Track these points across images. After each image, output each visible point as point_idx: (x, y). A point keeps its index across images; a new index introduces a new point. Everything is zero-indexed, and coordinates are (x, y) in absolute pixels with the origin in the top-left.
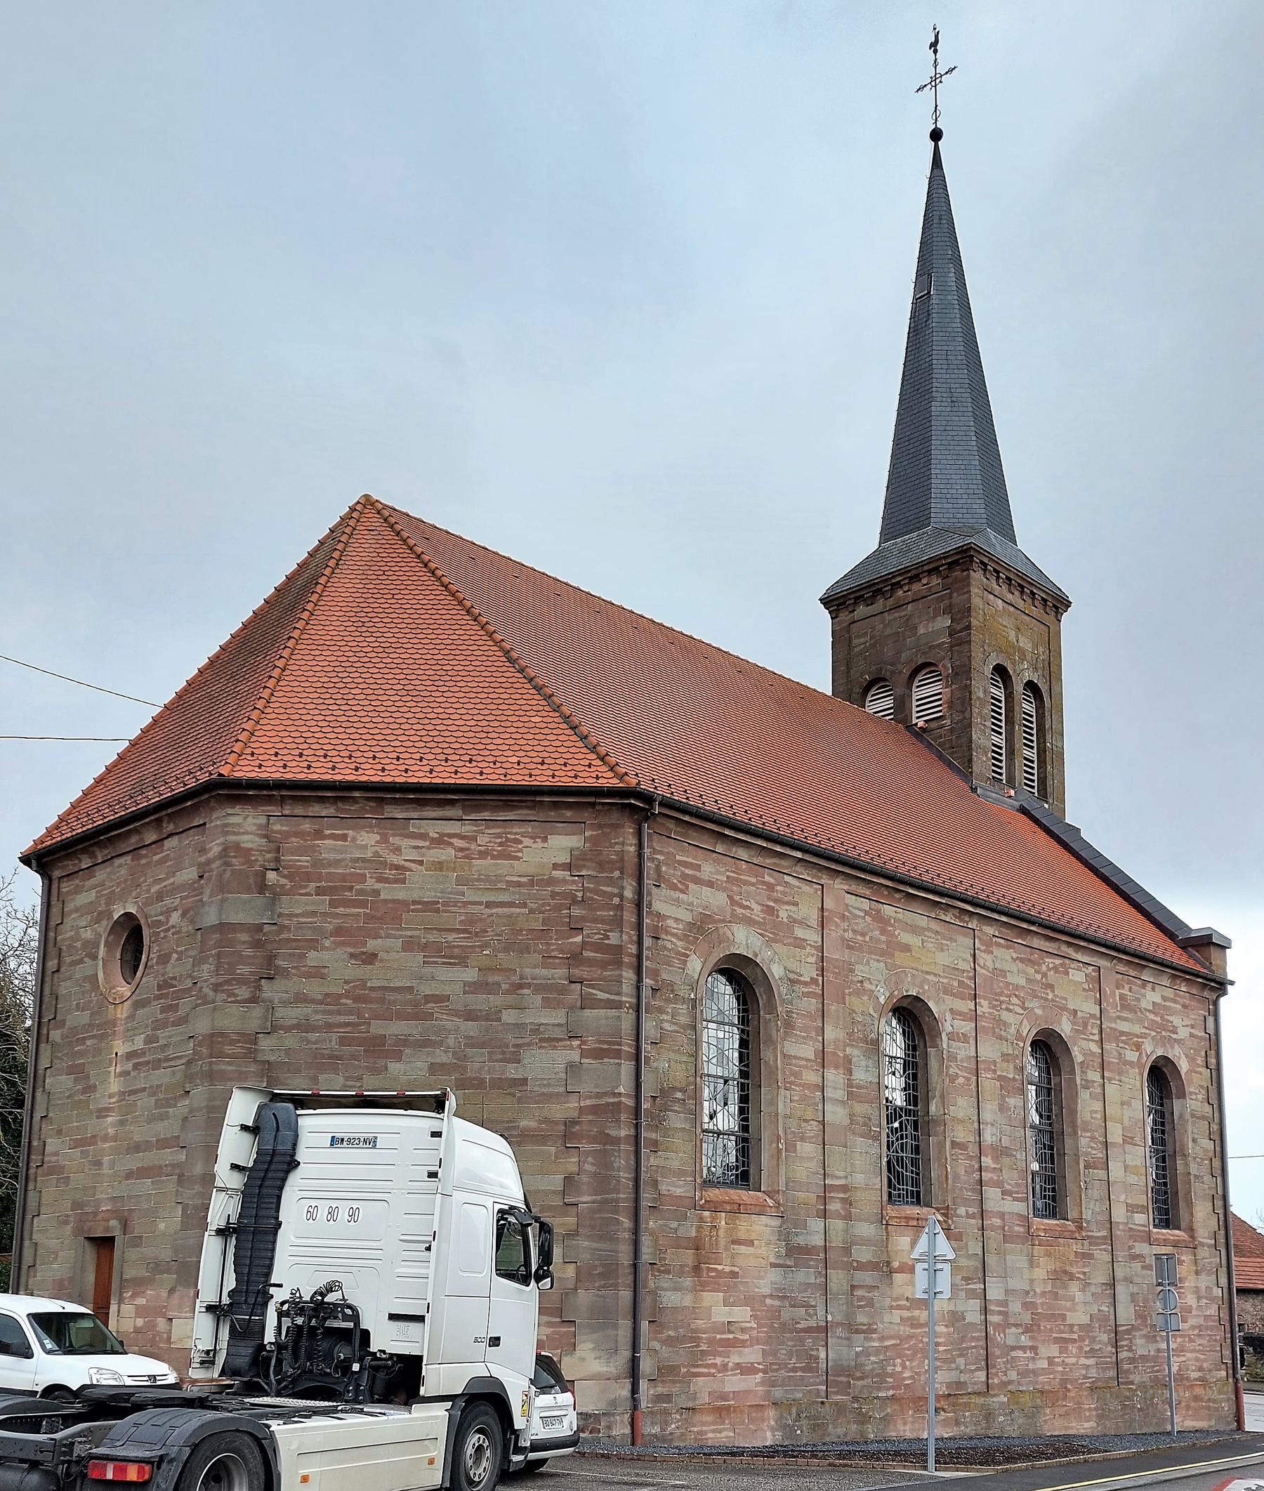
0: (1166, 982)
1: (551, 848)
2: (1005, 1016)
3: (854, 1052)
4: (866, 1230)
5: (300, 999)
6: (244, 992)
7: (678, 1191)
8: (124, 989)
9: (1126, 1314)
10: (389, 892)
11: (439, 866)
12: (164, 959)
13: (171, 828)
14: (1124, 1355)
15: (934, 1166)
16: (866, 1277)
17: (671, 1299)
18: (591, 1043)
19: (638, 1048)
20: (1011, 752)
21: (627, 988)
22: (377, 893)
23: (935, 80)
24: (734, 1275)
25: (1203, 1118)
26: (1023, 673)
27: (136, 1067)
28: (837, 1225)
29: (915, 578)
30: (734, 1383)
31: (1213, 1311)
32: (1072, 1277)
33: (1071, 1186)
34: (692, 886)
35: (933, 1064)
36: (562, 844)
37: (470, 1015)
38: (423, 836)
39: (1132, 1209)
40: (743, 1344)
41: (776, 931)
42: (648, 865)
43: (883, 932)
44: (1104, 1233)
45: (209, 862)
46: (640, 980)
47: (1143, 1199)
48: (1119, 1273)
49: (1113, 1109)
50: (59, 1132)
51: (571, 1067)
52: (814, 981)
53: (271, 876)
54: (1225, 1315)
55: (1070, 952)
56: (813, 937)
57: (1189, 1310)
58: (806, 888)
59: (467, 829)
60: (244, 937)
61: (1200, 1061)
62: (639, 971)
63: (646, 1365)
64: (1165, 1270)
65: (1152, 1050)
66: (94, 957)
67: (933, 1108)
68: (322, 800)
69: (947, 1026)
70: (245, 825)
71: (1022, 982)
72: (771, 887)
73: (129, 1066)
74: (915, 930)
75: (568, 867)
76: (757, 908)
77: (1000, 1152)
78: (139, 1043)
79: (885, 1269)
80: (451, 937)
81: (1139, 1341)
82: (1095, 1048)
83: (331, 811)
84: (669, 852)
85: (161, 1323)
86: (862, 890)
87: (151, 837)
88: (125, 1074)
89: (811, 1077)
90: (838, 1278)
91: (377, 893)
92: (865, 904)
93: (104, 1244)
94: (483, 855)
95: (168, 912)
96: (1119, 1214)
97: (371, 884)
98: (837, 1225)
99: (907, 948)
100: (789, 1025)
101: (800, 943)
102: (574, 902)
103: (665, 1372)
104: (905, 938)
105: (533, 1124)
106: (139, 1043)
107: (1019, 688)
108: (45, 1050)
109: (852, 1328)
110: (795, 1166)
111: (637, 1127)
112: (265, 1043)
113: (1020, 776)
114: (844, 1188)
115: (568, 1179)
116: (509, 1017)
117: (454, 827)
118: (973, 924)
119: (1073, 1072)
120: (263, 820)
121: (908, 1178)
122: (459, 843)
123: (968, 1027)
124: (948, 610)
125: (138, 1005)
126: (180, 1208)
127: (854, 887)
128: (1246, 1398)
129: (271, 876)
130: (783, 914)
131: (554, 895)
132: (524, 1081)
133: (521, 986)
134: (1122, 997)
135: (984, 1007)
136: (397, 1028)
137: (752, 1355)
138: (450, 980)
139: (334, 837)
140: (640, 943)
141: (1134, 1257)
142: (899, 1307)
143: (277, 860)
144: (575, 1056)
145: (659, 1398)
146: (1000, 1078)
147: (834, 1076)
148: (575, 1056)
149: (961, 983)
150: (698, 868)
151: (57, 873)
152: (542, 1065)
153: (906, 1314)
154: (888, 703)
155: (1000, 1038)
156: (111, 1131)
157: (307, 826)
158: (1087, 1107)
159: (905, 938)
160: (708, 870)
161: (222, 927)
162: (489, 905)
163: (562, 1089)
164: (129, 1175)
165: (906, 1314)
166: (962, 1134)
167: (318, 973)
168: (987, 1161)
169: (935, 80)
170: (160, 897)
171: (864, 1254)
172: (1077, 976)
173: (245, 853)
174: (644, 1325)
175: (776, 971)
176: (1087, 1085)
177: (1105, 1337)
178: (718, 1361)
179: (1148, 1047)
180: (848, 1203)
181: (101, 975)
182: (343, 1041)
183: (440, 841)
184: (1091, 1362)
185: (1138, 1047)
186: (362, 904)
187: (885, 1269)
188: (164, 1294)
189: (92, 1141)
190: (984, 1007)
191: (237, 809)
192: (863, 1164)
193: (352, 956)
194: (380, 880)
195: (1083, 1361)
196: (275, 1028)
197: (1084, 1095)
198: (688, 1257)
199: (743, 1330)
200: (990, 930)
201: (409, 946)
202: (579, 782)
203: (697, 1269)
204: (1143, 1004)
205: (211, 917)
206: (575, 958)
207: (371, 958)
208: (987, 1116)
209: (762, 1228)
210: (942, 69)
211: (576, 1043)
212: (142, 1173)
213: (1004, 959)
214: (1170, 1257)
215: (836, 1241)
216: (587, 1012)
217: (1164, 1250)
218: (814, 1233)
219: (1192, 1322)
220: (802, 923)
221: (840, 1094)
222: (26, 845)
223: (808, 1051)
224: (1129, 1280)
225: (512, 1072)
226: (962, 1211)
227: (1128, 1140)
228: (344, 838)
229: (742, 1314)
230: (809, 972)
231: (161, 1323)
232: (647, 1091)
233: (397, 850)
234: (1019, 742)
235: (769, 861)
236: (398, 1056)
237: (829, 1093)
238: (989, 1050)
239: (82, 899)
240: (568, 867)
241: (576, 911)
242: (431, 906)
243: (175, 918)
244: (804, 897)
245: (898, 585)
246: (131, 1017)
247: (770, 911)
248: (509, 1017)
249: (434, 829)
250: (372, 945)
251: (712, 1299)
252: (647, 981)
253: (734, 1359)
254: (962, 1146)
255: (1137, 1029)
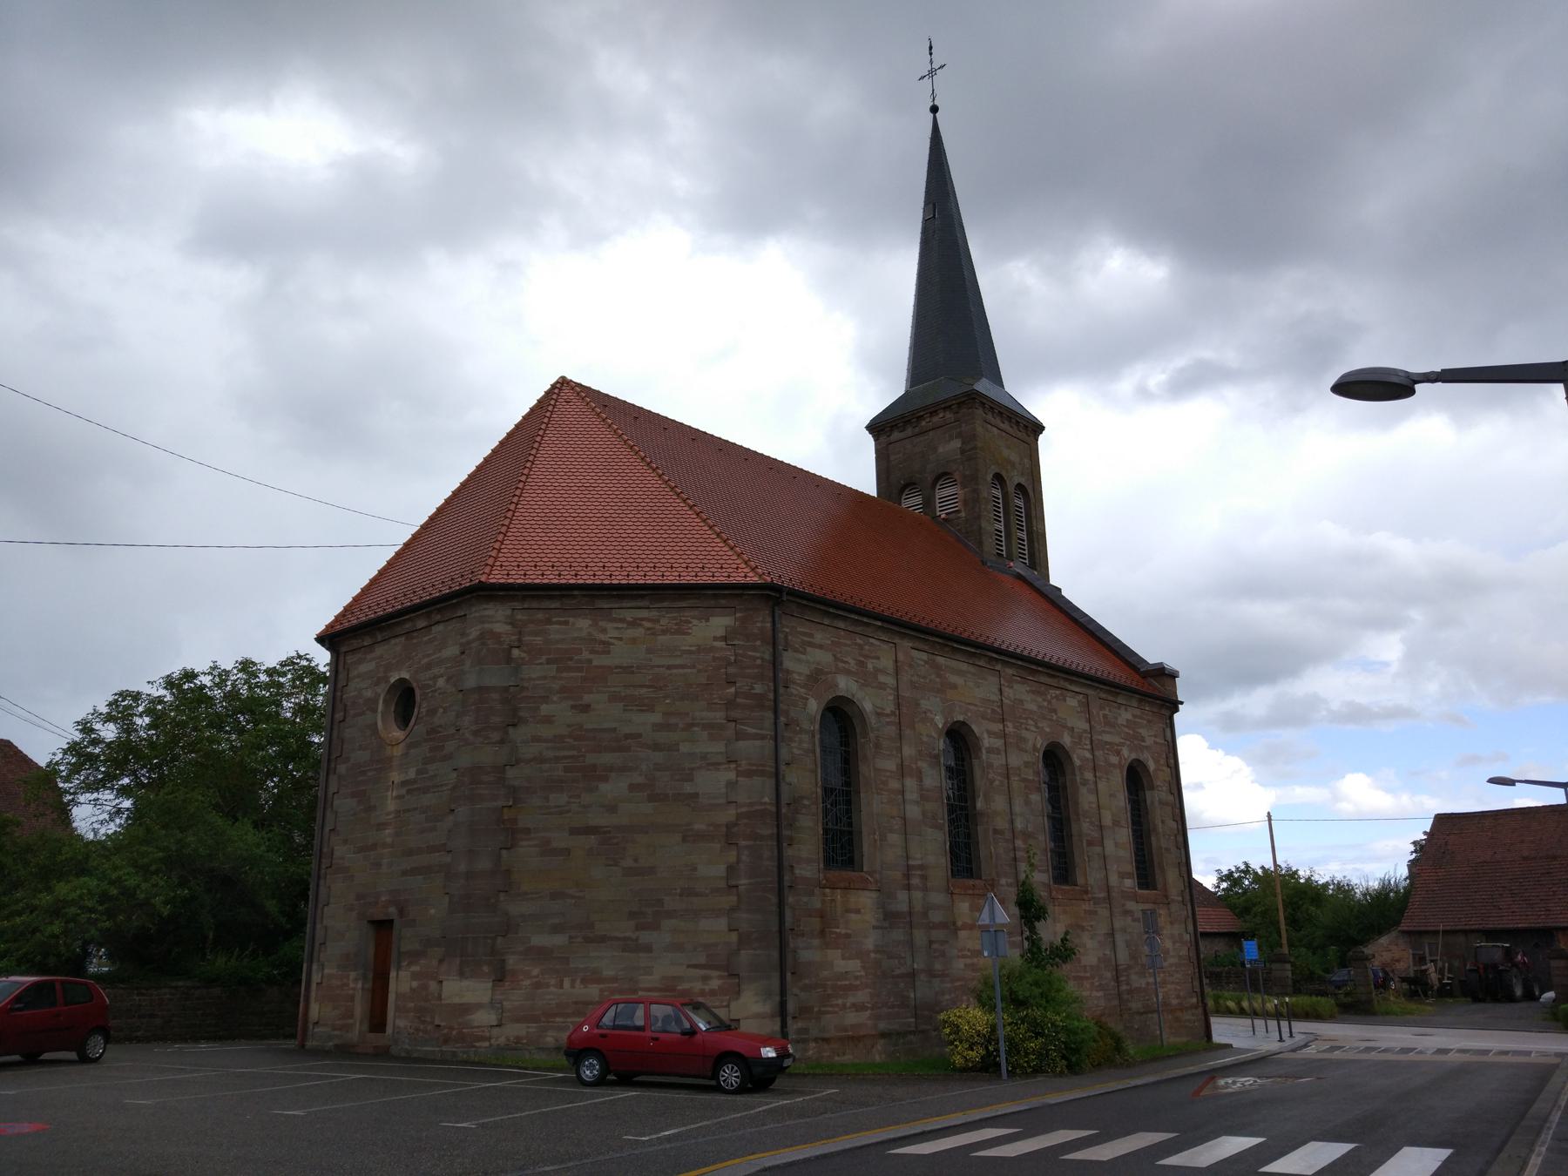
0: (1135, 704)
1: (714, 627)
2: (1025, 734)
3: (923, 765)
4: (938, 898)
5: (536, 739)
6: (496, 736)
7: (808, 874)
8: (398, 734)
9: (1123, 956)
10: (599, 661)
11: (634, 641)
12: (432, 712)
13: (438, 617)
14: (1124, 987)
15: (982, 847)
16: (938, 934)
17: (806, 955)
18: (744, 765)
19: (777, 768)
20: (1008, 535)
21: (769, 723)
22: (590, 661)
23: (932, 73)
24: (848, 936)
25: (1167, 804)
26: (1014, 478)
27: (408, 792)
28: (917, 895)
29: (932, 414)
30: (851, 1018)
31: (1184, 952)
32: (1083, 929)
33: (1077, 860)
34: (809, 649)
35: (978, 773)
36: (720, 623)
37: (656, 747)
38: (622, 620)
39: (1122, 875)
40: (856, 988)
41: (867, 679)
42: (781, 636)
43: (938, 676)
44: (1102, 895)
45: (469, 643)
46: (776, 718)
47: (1130, 867)
48: (1117, 925)
49: (1102, 799)
50: (345, 842)
51: (731, 785)
52: (893, 713)
53: (516, 652)
54: (1193, 954)
55: (1063, 683)
56: (890, 681)
57: (1167, 952)
58: (885, 646)
59: (654, 614)
60: (495, 696)
61: (1162, 761)
62: (776, 712)
63: (791, 1006)
64: (1150, 925)
65: (1128, 755)
66: (375, 711)
67: (980, 804)
68: (551, 597)
69: (987, 742)
70: (497, 618)
71: (1034, 708)
72: (861, 647)
73: (403, 791)
74: (960, 673)
75: (725, 638)
76: (852, 662)
77: (1027, 835)
78: (412, 774)
79: (952, 927)
80: (643, 691)
81: (1133, 977)
82: (1088, 755)
83: (556, 604)
84: (794, 627)
85: (433, 985)
86: (921, 646)
87: (421, 623)
88: (399, 797)
89: (894, 784)
90: (920, 936)
91: (590, 661)
92: (924, 656)
93: (382, 927)
94: (664, 632)
95: (435, 678)
96: (1114, 879)
97: (586, 655)
98: (917, 895)
99: (954, 687)
100: (878, 746)
101: (882, 686)
102: (729, 664)
103: (804, 1011)
104: (953, 679)
105: (703, 827)
106: (412, 774)
107: (1011, 489)
108: (333, 780)
109: (931, 973)
110: (882, 850)
111: (778, 826)
112: (511, 773)
113: (1015, 551)
114: (921, 867)
115: (731, 869)
116: (685, 748)
117: (644, 614)
118: (998, 667)
119: (1074, 774)
120: (509, 612)
121: (964, 859)
122: (647, 624)
123: (999, 743)
124: (959, 435)
125: (410, 746)
126: (447, 898)
127: (917, 645)
128: (1213, 1020)
129: (516, 652)
130: (870, 666)
131: (714, 659)
132: (696, 795)
133: (693, 725)
134: (1105, 716)
135: (1010, 728)
136: (607, 758)
137: (862, 996)
138: (643, 722)
139: (559, 623)
140: (776, 691)
141: (1127, 913)
142: (964, 957)
143: (520, 640)
144: (732, 776)
145: (800, 1031)
146: (1024, 780)
147: (910, 783)
148: (732, 776)
149: (993, 711)
150: (811, 636)
151: (343, 649)
152: (712, 783)
153: (969, 961)
154: (918, 500)
155: (1022, 750)
156: (389, 840)
157: (540, 616)
158: (1086, 799)
159: (953, 679)
160: (819, 637)
161: (481, 689)
162: (669, 667)
163: (722, 801)
164: (405, 873)
165: (969, 961)
166: (1001, 823)
167: (548, 720)
168: (1019, 843)
169: (932, 73)
170: (429, 666)
171: (936, 917)
172: (1072, 702)
173: (496, 636)
174: (789, 975)
175: (868, 706)
176: (1085, 782)
177: (1109, 975)
178: (840, 1002)
179: (1125, 752)
180: (924, 878)
181: (380, 724)
182: (566, 770)
183: (634, 623)
184: (1100, 994)
185: (1118, 753)
186: (580, 669)
187: (952, 927)
188: (435, 962)
189: (374, 846)
190: (1010, 728)
191: (491, 605)
192: (932, 849)
193: (573, 707)
194: (593, 652)
195: (1095, 994)
196: (518, 761)
197: (1083, 790)
198: (816, 923)
199: (857, 978)
200: (1010, 671)
201: (614, 698)
202: (732, 580)
203: (822, 933)
204: (1120, 721)
205: (471, 682)
206: (730, 704)
207: (586, 708)
208: (1017, 809)
209: (866, 900)
210: (936, 66)
211: (733, 766)
212: (414, 871)
213: (1020, 692)
214: (1153, 912)
215: (918, 907)
216: (741, 744)
217: (1147, 906)
218: (901, 902)
219: (1171, 961)
220: (884, 672)
221: (915, 796)
222: (320, 628)
223: (890, 765)
224: (1124, 930)
225: (688, 788)
226: (1003, 881)
227: (1116, 823)
228: (566, 623)
229: (854, 965)
230: (889, 708)
231: (433, 985)
232: (785, 799)
233: (604, 631)
234: (1014, 528)
235: (859, 629)
236: (605, 779)
237: (908, 796)
238: (1015, 760)
239: (364, 668)
240: (725, 638)
241: (732, 670)
242: (628, 670)
243: (441, 682)
244: (884, 655)
245: (920, 418)
246: (406, 755)
247: (862, 664)
248: (685, 748)
249: (629, 615)
250: (587, 698)
251: (834, 955)
252: (782, 719)
253: (851, 1000)
254: (1001, 832)
255: (1117, 740)
